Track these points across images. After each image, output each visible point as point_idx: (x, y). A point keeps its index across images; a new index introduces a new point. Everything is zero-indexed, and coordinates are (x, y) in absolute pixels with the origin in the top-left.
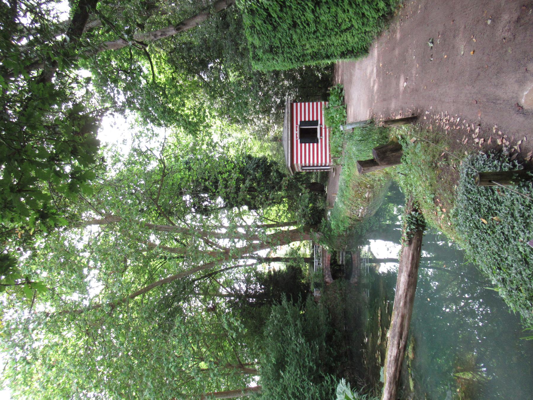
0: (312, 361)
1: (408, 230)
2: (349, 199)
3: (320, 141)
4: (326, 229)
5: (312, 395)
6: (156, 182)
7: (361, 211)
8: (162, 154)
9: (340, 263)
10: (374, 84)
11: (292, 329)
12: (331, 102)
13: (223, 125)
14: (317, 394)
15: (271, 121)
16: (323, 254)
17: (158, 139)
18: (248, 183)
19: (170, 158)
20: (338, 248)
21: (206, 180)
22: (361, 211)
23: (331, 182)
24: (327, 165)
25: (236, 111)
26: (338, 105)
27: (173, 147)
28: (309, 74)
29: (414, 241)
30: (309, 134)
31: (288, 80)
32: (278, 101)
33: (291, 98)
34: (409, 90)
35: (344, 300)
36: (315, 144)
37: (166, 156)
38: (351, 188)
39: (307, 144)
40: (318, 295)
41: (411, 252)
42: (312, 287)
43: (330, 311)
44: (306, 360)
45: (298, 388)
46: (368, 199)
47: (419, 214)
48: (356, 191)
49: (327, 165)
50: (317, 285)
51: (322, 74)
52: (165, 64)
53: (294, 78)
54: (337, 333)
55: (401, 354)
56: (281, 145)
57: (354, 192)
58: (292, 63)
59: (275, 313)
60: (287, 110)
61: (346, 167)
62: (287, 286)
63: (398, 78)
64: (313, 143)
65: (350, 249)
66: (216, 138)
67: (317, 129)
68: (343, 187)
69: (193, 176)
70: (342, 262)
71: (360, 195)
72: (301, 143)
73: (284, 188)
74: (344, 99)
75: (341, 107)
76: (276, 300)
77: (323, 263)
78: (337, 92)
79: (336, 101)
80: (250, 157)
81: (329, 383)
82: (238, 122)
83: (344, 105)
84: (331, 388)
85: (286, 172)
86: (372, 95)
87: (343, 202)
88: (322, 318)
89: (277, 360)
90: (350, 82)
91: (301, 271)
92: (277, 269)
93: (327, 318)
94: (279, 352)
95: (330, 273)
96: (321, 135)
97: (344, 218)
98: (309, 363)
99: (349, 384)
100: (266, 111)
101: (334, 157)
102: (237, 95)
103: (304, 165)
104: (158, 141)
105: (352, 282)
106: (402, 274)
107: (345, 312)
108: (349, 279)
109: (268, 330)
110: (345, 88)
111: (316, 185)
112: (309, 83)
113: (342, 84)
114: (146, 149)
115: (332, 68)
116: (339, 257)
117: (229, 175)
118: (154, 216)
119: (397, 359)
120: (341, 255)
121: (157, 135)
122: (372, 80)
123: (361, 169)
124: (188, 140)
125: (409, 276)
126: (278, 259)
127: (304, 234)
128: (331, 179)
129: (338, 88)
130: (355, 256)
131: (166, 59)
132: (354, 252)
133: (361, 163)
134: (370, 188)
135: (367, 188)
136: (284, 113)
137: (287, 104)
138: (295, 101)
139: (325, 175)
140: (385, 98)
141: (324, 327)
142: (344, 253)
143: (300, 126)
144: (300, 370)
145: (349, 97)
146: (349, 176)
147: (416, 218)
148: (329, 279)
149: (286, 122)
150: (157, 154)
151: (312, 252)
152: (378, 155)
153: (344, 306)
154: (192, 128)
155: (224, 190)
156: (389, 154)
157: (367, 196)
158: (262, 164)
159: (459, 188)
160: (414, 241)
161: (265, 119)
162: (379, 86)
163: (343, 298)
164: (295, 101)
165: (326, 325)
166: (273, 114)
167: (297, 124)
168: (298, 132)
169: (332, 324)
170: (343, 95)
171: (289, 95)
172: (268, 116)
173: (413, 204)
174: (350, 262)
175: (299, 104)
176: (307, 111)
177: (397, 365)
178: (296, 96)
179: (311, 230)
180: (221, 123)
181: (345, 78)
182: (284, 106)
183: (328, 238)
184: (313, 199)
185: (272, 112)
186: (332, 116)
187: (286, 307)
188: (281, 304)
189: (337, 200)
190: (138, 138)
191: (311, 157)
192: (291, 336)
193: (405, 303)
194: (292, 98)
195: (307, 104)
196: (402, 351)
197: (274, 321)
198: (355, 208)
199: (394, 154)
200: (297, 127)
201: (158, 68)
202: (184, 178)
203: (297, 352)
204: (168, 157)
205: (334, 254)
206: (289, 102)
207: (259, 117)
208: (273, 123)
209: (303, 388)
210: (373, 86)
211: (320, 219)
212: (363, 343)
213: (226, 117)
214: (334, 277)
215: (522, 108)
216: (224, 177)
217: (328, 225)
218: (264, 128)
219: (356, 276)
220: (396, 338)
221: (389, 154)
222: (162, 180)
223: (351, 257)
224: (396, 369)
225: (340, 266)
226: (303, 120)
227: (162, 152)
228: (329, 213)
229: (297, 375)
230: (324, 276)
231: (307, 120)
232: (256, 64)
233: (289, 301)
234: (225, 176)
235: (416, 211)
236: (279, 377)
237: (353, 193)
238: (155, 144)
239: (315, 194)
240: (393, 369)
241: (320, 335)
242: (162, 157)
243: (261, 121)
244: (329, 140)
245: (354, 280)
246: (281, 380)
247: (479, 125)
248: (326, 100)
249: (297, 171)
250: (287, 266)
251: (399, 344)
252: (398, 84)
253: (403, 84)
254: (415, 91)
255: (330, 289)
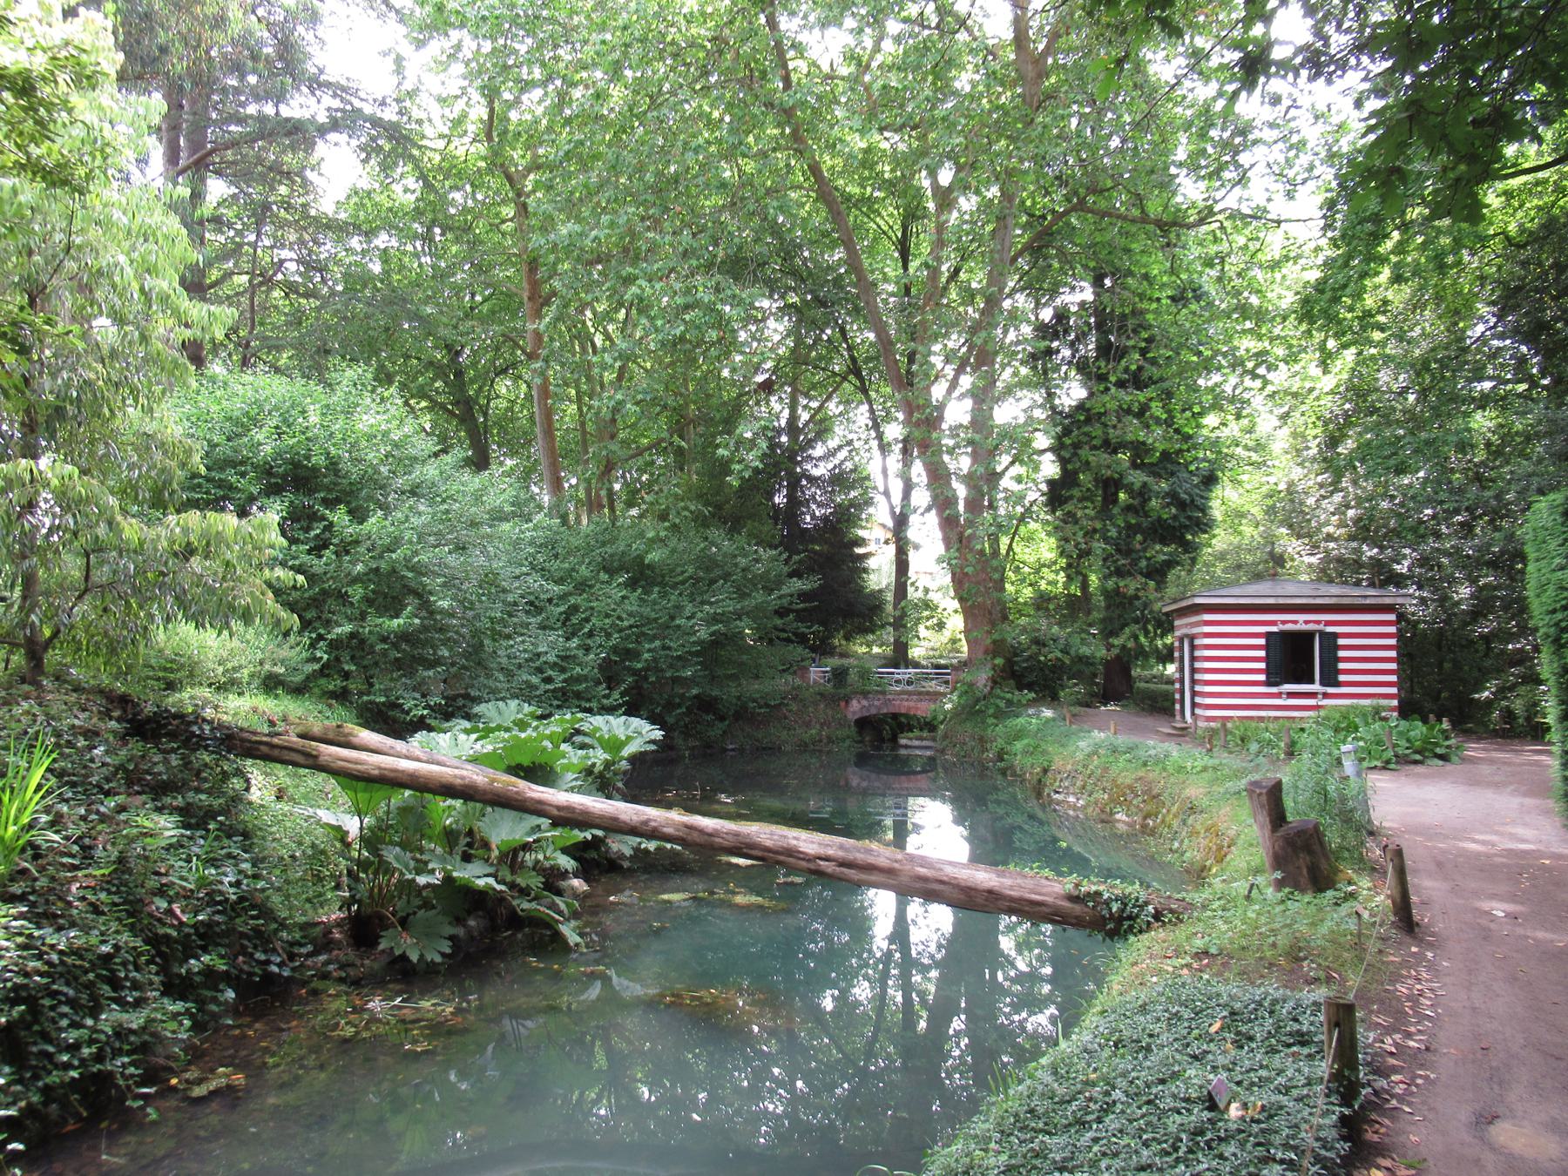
0: (655, 660)
1: (1106, 896)
2: (1106, 770)
3: (1274, 690)
4: (1002, 704)
5: (575, 656)
6: (1139, 200)
7: (1071, 799)
8: (1231, 217)
9: (903, 742)
10: (1483, 843)
11: (730, 606)
12: (1404, 724)
13: (1318, 398)
14: (578, 669)
15: (1332, 545)
16: (928, 693)
17: (1279, 198)
18: (1137, 478)
19: (1216, 240)
20: (945, 737)
21: (1143, 352)
22: (1071, 799)
23: (1140, 720)
24: (1198, 711)
25: (1365, 437)
26: (1395, 745)
27: (1253, 246)
28: (1488, 663)
29: (1077, 909)
30: (1293, 658)
31: (1472, 596)
32: (1402, 568)
33: (1411, 607)
34: (1484, 922)
35: (803, 747)
36: (1262, 677)
37: (1222, 228)
38: (1141, 774)
39: (1262, 653)
40: (812, 676)
41: (1049, 899)
42: (835, 661)
43: (774, 710)
44: (657, 643)
45: (587, 620)
46: (1107, 820)
47: (1149, 923)
48: (1131, 787)
49: (1198, 711)
50: (839, 675)
51: (1489, 703)
52: (1539, 208)
53: (1476, 614)
54: (720, 727)
55: (804, 864)
56: (1258, 577)
57: (1128, 781)
58: (1554, 611)
59: (766, 559)
60: (1372, 595)
61: (1208, 761)
62: (832, 594)
63: (1512, 898)
64: (1267, 671)
65: (946, 769)
66: (1280, 378)
67: (1312, 681)
68: (1141, 753)
69: (1157, 312)
70: (906, 747)
71: (1121, 796)
72: (1268, 635)
73: (1121, 584)
74: (1416, 762)
75: (1390, 753)
76: (800, 562)
77: (903, 692)
78: (1436, 744)
79: (1408, 740)
80: (1210, 480)
81: (605, 701)
82: (1333, 441)
83: (1397, 763)
84: (594, 705)
85: (1171, 591)
86: (1446, 837)
87: (1095, 753)
88: (755, 688)
89: (650, 567)
90: (1474, 782)
91: (865, 631)
92: (872, 563)
93: (754, 701)
94: (672, 571)
95: (873, 711)
96: (1291, 695)
97: (1044, 753)
98: (649, 651)
99: (653, 747)
100: (1363, 531)
101: (1227, 732)
102: (1428, 443)
103: (1197, 642)
104: (1269, 200)
105: (849, 770)
106: (993, 876)
107: (773, 750)
108: (857, 765)
109: (721, 543)
110: (1449, 767)
111: (1123, 682)
112: (1454, 661)
113: (1464, 760)
114: (1247, 166)
115: (1537, 732)
116: (920, 738)
117: (1158, 421)
118: (1034, 203)
119: (791, 852)
120: (925, 743)
121: (1290, 195)
122: (1494, 838)
123: (1261, 787)
124: (1283, 293)
125: (990, 892)
126: (902, 566)
127: (988, 641)
128: (1149, 721)
129: (1448, 747)
130: (923, 781)
131: (1556, 211)
132: (934, 780)
133: (1275, 791)
134: (1144, 826)
135: (1145, 818)
136: (1358, 584)
137: (1390, 595)
138: (1401, 617)
139: (1160, 704)
140: (1441, 866)
141: (734, 692)
142: (928, 753)
143: (1322, 633)
144: (631, 627)
145: (1426, 776)
146: (1181, 769)
147: (1137, 916)
148: (856, 708)
149: (1333, 592)
150: (1231, 200)
151: (924, 663)
152: (1300, 833)
153: (788, 748)
154: (1319, 307)
155: (1112, 405)
156: (1303, 860)
157: (1118, 816)
158: (1189, 518)
159: (1272, 989)
160: (1077, 909)
161: (1338, 527)
162: (1478, 855)
163: (806, 745)
164: (1401, 617)
165: (739, 698)
166: (1358, 551)
167: (1328, 623)
168: (1301, 627)
169: (742, 714)
170: (1429, 762)
171: (1423, 601)
172: (1351, 538)
173: (1172, 911)
174: (901, 767)
175: (1393, 629)
176: (1370, 656)
177: (777, 852)
178: (1418, 622)
179: (999, 661)
180: (1326, 389)
181: (1485, 769)
182: (1383, 584)
183: (972, 710)
184: (1083, 667)
185: (1365, 547)
186: (1356, 730)
187: (785, 590)
188: (791, 575)
189: (1098, 735)
190: (1284, 139)
191: (1223, 665)
192: (711, 604)
193: (925, 879)
194: (1412, 609)
195: (1393, 654)
196: (812, 866)
197: (745, 556)
198: (1079, 783)
199: (1305, 871)
200: (1318, 622)
201: (1528, 190)
202: (1151, 284)
203: (673, 618)
204: (1218, 233)
205: (927, 724)
206: (1400, 600)
207: (1348, 507)
208: (1326, 551)
209: (591, 634)
210: (1474, 841)
211: (1030, 687)
212: (716, 791)
213: (1347, 406)
214: (863, 723)
215: (1490, 1123)
216: (1153, 404)
217: (1012, 709)
218: (1313, 524)
219: (865, 784)
220: (841, 854)
221: (1303, 860)
222: (1144, 219)
223: (915, 773)
224: (768, 850)
225: (894, 739)
226: (1341, 642)
227: (1235, 215)
228: (1048, 713)
229: (620, 618)
230: (865, 694)
231: (1341, 654)
232: (1552, 507)
233: (799, 596)
234: (1156, 409)
235: (1157, 916)
236: (612, 572)
237: (1127, 778)
238: (1259, 191)
239: (1095, 676)
240: (769, 843)
241: (713, 678)
242: (1220, 217)
243: (1332, 516)
244: (1276, 718)
245: (855, 778)
246: (604, 576)
247: (1427, 1049)
248: (1406, 710)
249: (1177, 623)
250: (880, 591)
251: (827, 859)
252: (1494, 897)
253: (1499, 910)
254: (1486, 935)
255: (830, 712)
